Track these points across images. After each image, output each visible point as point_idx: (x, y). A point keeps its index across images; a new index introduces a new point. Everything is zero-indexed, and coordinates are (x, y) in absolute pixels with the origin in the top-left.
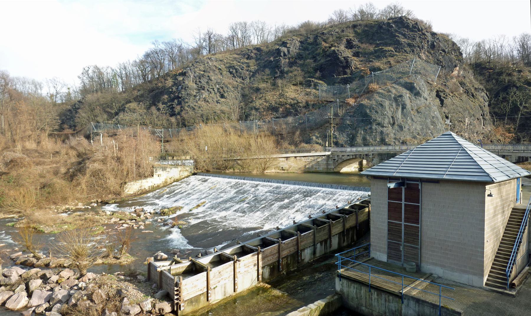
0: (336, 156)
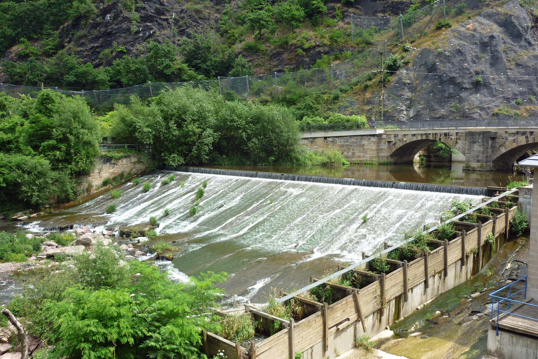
0: (392, 136)
